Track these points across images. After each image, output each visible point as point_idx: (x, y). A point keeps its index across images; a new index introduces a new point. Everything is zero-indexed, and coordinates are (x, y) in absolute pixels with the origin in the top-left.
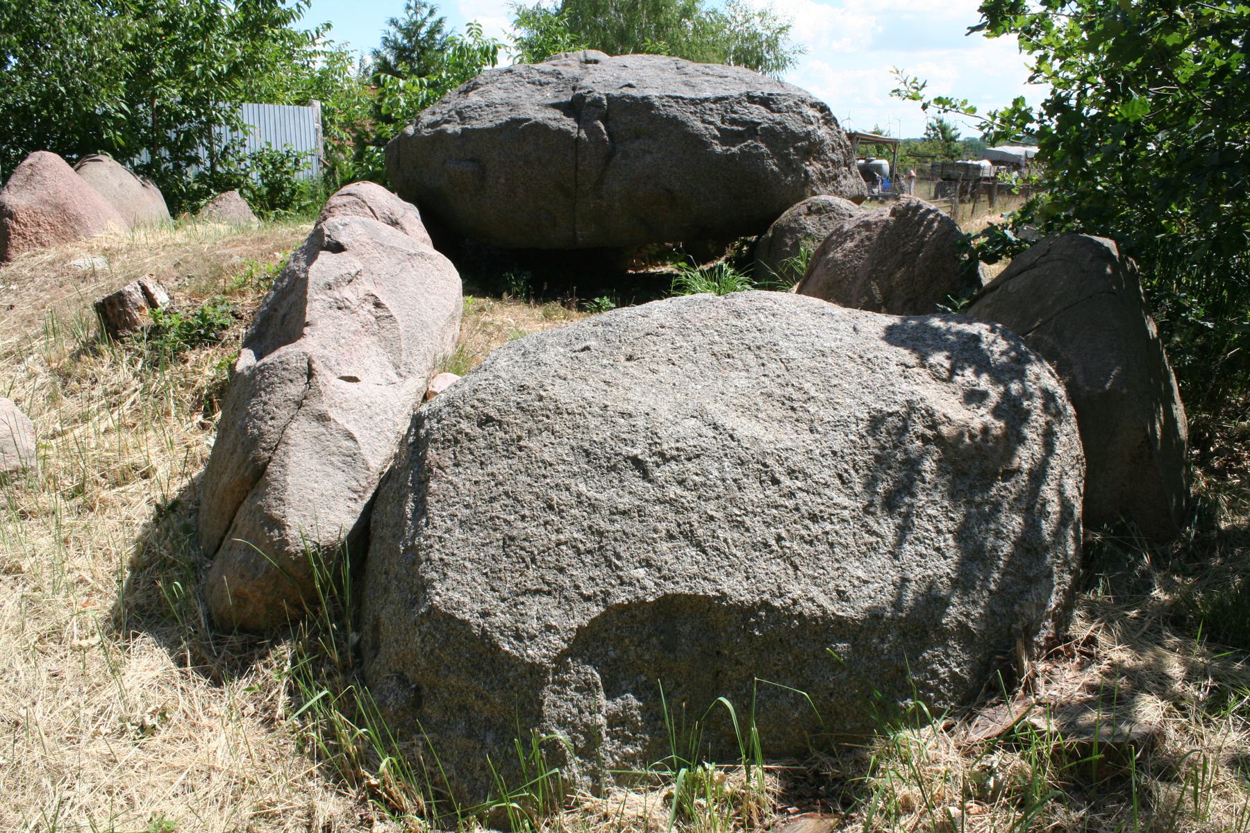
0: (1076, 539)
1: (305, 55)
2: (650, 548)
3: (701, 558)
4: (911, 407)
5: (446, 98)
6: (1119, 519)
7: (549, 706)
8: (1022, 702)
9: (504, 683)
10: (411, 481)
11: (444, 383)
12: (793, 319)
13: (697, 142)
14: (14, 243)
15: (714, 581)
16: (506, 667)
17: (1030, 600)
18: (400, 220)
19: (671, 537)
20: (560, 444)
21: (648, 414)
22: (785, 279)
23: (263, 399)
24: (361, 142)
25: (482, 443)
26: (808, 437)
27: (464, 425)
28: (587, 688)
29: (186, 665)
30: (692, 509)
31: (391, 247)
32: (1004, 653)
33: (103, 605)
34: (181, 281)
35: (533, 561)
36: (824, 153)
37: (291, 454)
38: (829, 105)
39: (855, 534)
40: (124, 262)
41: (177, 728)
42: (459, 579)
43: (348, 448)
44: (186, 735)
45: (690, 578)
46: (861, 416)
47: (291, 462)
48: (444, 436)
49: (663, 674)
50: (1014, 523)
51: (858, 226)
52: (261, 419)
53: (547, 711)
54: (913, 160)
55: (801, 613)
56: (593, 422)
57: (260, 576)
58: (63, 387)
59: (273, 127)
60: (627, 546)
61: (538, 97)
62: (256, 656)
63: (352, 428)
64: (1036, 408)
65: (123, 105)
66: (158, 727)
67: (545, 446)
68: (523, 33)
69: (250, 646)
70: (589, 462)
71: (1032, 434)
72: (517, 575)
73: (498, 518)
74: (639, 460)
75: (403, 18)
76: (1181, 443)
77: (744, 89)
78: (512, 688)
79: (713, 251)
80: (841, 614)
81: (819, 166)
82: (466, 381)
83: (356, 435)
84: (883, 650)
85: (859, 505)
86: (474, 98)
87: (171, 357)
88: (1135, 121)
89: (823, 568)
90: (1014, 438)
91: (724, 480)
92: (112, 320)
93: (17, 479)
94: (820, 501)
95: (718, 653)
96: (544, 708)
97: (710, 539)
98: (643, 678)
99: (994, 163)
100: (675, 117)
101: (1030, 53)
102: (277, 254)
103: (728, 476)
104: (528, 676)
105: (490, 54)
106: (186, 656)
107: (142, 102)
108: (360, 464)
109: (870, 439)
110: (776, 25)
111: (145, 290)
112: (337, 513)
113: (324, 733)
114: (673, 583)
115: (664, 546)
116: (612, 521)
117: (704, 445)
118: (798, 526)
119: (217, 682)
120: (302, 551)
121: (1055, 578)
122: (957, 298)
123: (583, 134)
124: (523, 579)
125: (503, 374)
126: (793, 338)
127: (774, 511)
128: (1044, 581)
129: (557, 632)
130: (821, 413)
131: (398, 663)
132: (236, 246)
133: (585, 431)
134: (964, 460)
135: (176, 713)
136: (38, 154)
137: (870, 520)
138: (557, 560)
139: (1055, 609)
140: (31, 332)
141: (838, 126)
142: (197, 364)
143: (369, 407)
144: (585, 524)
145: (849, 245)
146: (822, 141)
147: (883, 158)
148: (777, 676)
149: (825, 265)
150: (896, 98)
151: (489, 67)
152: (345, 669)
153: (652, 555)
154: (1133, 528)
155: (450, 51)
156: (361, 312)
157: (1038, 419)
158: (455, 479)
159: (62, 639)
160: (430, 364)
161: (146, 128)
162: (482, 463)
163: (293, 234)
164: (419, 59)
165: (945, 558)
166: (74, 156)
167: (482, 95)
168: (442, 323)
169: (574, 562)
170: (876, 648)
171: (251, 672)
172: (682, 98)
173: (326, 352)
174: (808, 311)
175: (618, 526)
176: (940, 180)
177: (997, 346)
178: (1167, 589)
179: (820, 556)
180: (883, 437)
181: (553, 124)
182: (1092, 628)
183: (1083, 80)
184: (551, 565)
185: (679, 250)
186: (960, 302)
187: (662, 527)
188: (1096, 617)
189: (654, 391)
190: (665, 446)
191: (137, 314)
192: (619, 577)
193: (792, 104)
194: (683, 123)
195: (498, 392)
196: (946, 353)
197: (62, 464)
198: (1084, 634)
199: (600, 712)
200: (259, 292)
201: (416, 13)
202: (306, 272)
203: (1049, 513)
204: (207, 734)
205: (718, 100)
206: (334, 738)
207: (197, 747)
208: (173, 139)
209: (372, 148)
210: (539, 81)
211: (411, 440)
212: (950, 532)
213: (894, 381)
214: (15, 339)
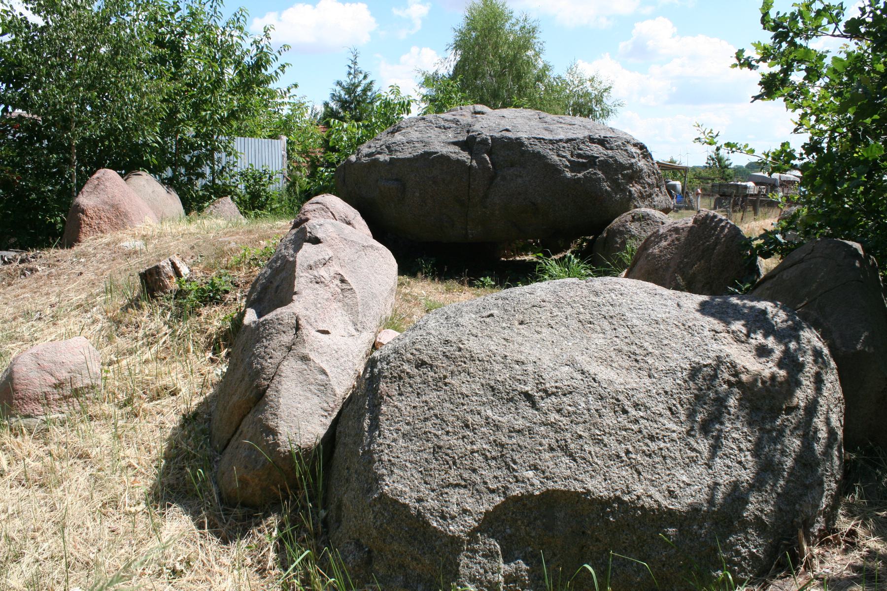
0: (840, 458)
1: (277, 105)
2: (537, 457)
6: (868, 444)
7: (463, 567)
8: (804, 576)
9: (432, 550)
10: (368, 405)
11: (388, 337)
12: (635, 297)
13: (554, 170)
14: (84, 230)
15: (582, 481)
16: (434, 538)
17: (807, 501)
18: (352, 222)
19: (552, 449)
20: (474, 381)
21: (535, 362)
22: (616, 267)
23: (265, 344)
24: (314, 165)
25: (418, 380)
26: (647, 381)
27: (406, 367)
28: (490, 555)
29: (204, 528)
30: (567, 429)
31: (352, 241)
32: (788, 540)
33: (144, 485)
34: (195, 259)
36: (642, 178)
37: (283, 383)
38: (646, 145)
39: (681, 450)
42: (402, 474)
43: (321, 380)
44: (204, 578)
45: (565, 479)
46: (685, 367)
47: (283, 388)
48: (391, 374)
50: (795, 443)
51: (670, 231)
52: (263, 358)
53: (462, 570)
54: (699, 182)
55: (643, 506)
56: (497, 367)
57: (258, 467)
59: (253, 153)
60: (520, 455)
61: (443, 137)
62: (253, 524)
63: (324, 366)
64: (808, 363)
65: (158, 138)
66: (184, 571)
67: (463, 383)
69: (248, 517)
70: (494, 395)
71: (807, 383)
72: (443, 473)
73: (430, 433)
74: (529, 394)
75: (346, 80)
77: (587, 133)
78: (438, 553)
79: (561, 246)
80: (671, 507)
82: (406, 336)
83: (328, 371)
84: (701, 534)
85: (684, 430)
86: (398, 137)
87: (190, 312)
88: (873, 159)
89: (658, 474)
90: (793, 383)
91: (589, 410)
92: (151, 285)
93: (87, 393)
95: (583, 533)
96: (460, 568)
97: (579, 451)
98: (530, 549)
99: (757, 184)
100: (539, 152)
101: (793, 111)
103: (592, 407)
104: (449, 545)
105: (405, 107)
106: (204, 522)
107: (169, 136)
108: (329, 391)
109: (691, 383)
110: (603, 87)
111: (174, 265)
112: (313, 425)
113: (302, 581)
114: (553, 482)
115: (547, 456)
116: (510, 437)
117: (575, 385)
118: (641, 444)
119: (225, 542)
120: (289, 451)
121: (825, 486)
122: (742, 283)
123: (474, 163)
124: (447, 476)
125: (433, 332)
126: (635, 311)
127: (624, 433)
129: (471, 514)
130: (657, 364)
131: (356, 532)
132: (232, 235)
133: (491, 373)
134: (757, 399)
135: (197, 562)
136: (102, 171)
137: (691, 441)
138: (471, 463)
139: (825, 508)
140: (95, 291)
141: (652, 159)
142: (208, 317)
143: (336, 352)
144: (491, 438)
145: (664, 244)
146: (641, 170)
147: (677, 180)
148: (625, 551)
149: (646, 258)
150: (698, 143)
152: (316, 535)
153: (538, 461)
154: (879, 451)
155: (378, 103)
157: (810, 369)
158: (399, 405)
159: (117, 506)
161: (171, 153)
162: (418, 394)
163: (271, 228)
164: (356, 109)
165: (745, 469)
166: (123, 172)
169: (483, 465)
170: (696, 533)
171: (249, 535)
172: (543, 139)
173: (308, 313)
174: (645, 292)
175: (514, 441)
176: (718, 196)
177: (778, 316)
179: (657, 466)
180: (700, 382)
182: (853, 523)
183: (833, 130)
184: (467, 467)
185: (537, 244)
186: (744, 286)
187: (545, 442)
188: (855, 515)
189: (539, 346)
190: (548, 385)
191: (168, 281)
192: (515, 477)
193: (620, 144)
194: (544, 156)
195: (429, 344)
196: (743, 322)
197: (117, 383)
198: (848, 528)
200: (250, 268)
201: (355, 77)
203: (820, 438)
204: (218, 578)
205: (568, 141)
206: (309, 584)
207: (211, 587)
208: (188, 161)
209: (322, 169)
210: (444, 126)
211: (367, 376)
212: (748, 450)
213: (707, 342)
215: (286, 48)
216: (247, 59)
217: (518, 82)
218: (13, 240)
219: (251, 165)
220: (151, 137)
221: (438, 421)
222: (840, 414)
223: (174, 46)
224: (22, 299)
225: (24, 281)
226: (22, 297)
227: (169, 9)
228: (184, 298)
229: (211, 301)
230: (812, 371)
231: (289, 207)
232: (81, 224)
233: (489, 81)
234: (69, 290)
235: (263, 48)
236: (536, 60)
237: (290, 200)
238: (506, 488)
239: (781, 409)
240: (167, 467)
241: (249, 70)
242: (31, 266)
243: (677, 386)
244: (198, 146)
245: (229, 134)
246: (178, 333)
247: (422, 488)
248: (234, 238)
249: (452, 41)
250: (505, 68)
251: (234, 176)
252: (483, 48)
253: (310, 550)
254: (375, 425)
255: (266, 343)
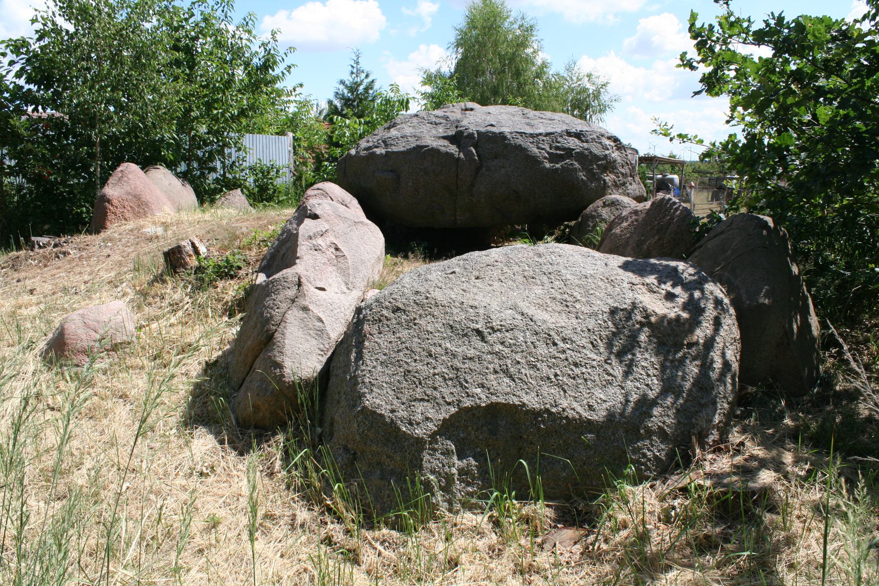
1: (283, 103)
3: (512, 384)
4: (634, 305)
5: (376, 132)
7: (426, 462)
11: (372, 294)
13: (534, 161)
14: (110, 218)
19: (496, 372)
20: (437, 322)
24: (319, 160)
25: (394, 321)
26: (574, 321)
27: (385, 312)
28: (447, 453)
32: (686, 446)
34: (210, 242)
35: (420, 383)
36: (616, 168)
38: (620, 138)
39: (599, 375)
40: (174, 231)
41: (219, 476)
43: (318, 327)
44: (225, 479)
46: (604, 310)
47: (288, 332)
49: (490, 448)
50: (693, 369)
51: (630, 213)
52: (272, 308)
53: (425, 465)
55: (567, 416)
56: (455, 311)
58: (144, 301)
59: (261, 149)
61: (434, 132)
68: (428, 89)
75: (348, 80)
76: (813, 339)
77: (565, 128)
80: (590, 418)
81: (613, 176)
83: (324, 319)
86: (394, 132)
90: (695, 322)
91: (526, 342)
94: (580, 356)
95: (521, 437)
96: (423, 463)
98: (479, 450)
100: (520, 145)
102: (269, 226)
103: (528, 340)
105: (404, 104)
108: (325, 336)
111: (193, 245)
115: (492, 377)
116: (464, 363)
121: (718, 405)
123: (462, 156)
125: (407, 285)
127: (554, 360)
128: (711, 406)
129: (432, 421)
130: (583, 308)
134: (664, 336)
139: (718, 423)
144: (449, 364)
145: (625, 224)
146: (615, 161)
147: (674, 174)
150: (654, 134)
151: (404, 112)
153: (485, 381)
156: (327, 252)
157: (710, 312)
158: (379, 341)
160: (365, 284)
161: (184, 149)
162: (394, 332)
163: (278, 215)
164: (358, 106)
165: (652, 390)
167: (398, 130)
168: (373, 261)
169: (442, 384)
175: (467, 366)
178: (793, 419)
181: (443, 149)
187: (491, 366)
190: (494, 324)
192: (467, 393)
195: (403, 294)
199: (454, 467)
201: (357, 76)
202: (297, 230)
209: (326, 163)
211: (355, 321)
212: (655, 376)
214: (113, 274)
215: (292, 50)
216: (255, 61)
217: (517, 79)
218: (46, 227)
219: (260, 160)
220: (168, 134)
221: (409, 352)
222: (736, 351)
223: (188, 50)
224: (58, 278)
225: (59, 263)
226: (58, 276)
227: (184, 14)
228: (202, 273)
229: (226, 276)
230: (711, 316)
231: (295, 199)
232: (107, 213)
233: (488, 77)
234: (99, 270)
235: (270, 50)
236: (535, 57)
237: (296, 193)
238: (460, 401)
239: (683, 345)
240: (193, 401)
241: (257, 71)
242: (64, 250)
243: (598, 326)
244: (210, 143)
245: (239, 131)
246: (198, 302)
247: (395, 402)
248: (245, 224)
249: (453, 39)
250: (504, 65)
251: (243, 170)
252: (483, 45)
253: (308, 447)
254: (360, 356)
255: (274, 297)
